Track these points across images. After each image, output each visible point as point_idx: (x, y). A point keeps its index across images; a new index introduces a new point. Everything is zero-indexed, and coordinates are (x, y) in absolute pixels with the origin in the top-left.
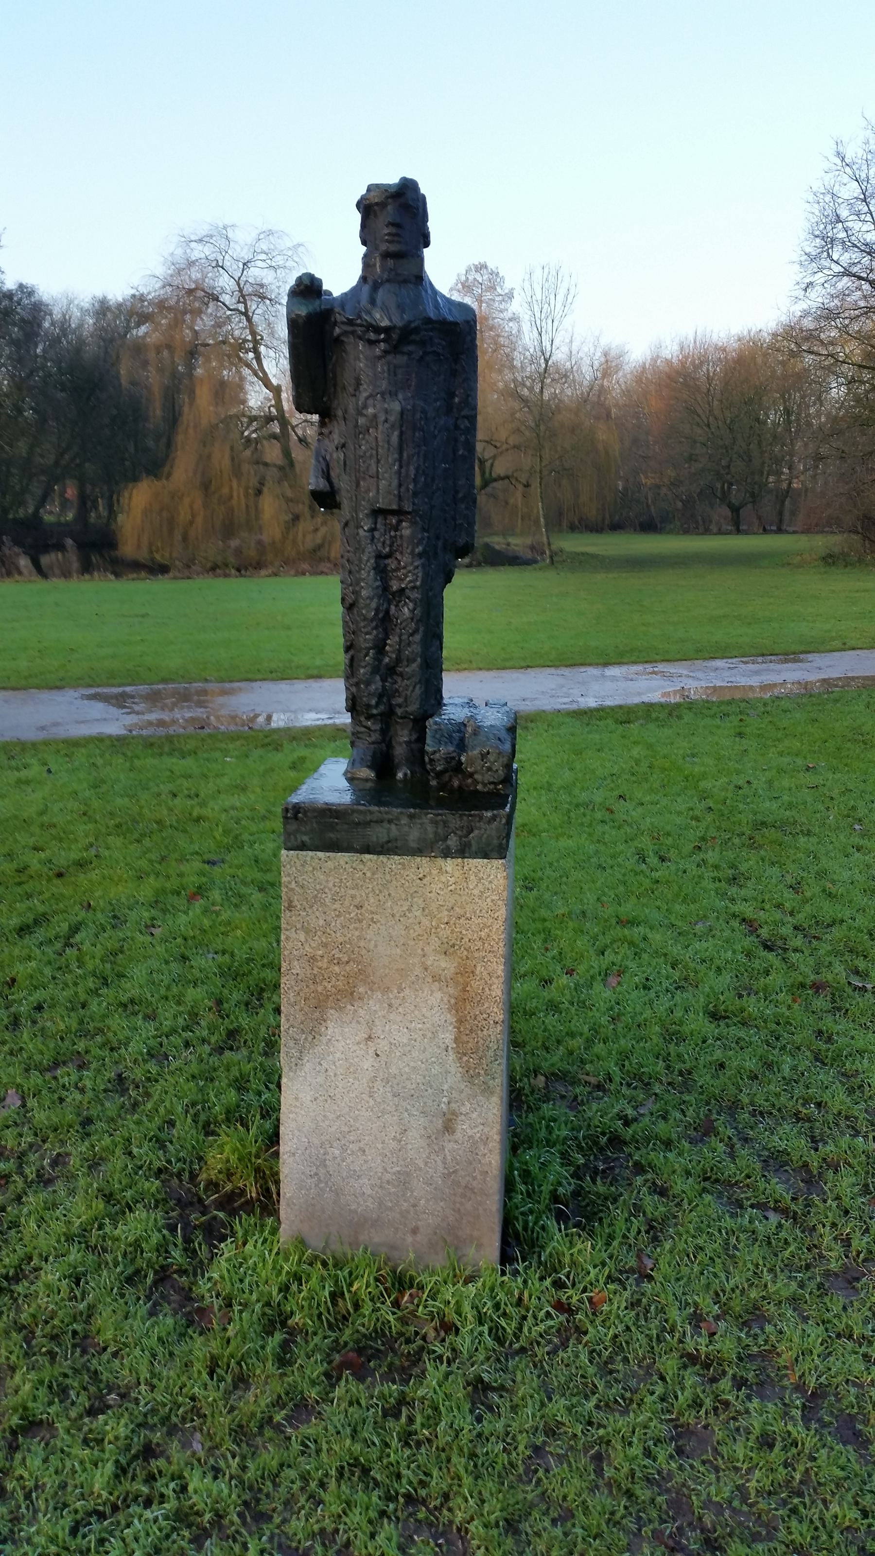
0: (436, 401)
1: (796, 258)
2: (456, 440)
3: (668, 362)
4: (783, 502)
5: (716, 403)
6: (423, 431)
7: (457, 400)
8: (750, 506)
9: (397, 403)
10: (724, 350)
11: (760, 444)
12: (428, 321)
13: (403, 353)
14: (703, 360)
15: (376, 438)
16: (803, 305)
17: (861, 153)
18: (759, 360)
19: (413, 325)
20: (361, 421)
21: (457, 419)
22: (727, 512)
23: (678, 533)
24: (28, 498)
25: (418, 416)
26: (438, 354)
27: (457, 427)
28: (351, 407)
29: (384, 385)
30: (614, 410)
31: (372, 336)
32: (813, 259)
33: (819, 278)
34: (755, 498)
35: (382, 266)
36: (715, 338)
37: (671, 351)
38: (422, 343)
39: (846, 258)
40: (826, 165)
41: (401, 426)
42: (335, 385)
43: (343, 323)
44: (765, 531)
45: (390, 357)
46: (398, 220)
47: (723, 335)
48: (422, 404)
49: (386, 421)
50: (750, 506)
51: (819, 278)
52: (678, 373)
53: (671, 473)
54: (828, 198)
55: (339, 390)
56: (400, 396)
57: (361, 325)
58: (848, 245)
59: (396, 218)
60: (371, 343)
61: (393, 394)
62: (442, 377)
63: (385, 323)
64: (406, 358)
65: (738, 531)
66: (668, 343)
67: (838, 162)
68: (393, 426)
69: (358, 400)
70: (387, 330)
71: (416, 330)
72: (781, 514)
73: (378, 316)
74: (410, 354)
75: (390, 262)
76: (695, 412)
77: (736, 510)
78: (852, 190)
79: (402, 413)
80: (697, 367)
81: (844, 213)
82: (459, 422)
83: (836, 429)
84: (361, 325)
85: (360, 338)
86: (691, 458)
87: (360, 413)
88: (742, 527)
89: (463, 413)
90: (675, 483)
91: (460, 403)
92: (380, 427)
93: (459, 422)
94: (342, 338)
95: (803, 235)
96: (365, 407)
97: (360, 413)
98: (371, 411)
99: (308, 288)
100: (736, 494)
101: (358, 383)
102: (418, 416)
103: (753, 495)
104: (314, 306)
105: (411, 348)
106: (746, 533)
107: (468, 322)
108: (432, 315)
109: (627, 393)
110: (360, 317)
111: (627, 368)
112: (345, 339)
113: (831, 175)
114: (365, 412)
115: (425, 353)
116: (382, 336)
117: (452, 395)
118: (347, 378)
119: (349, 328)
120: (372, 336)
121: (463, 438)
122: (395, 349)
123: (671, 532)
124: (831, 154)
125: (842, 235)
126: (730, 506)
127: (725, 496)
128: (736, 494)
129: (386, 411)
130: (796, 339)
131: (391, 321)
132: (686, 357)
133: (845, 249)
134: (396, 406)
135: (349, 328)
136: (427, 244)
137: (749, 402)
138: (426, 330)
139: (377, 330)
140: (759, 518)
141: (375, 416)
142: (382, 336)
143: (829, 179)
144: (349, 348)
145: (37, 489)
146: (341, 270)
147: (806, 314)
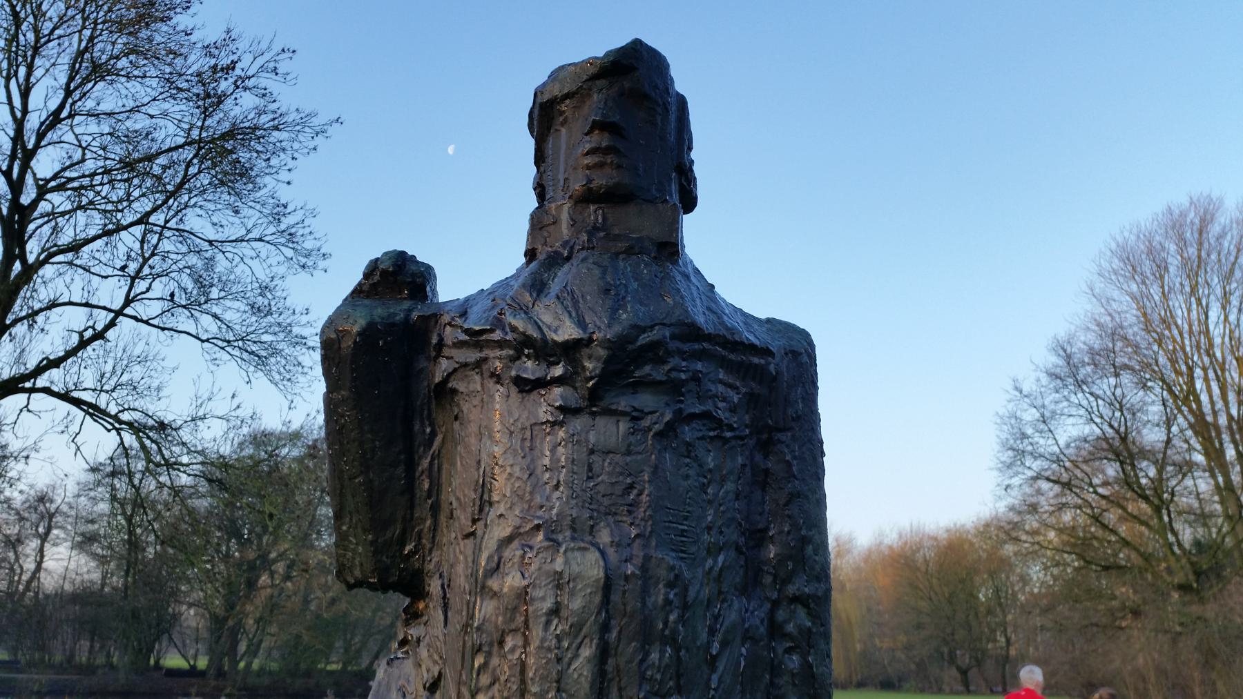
0: (713, 551)
1: (992, 465)
2: (775, 669)
3: (891, 548)
4: (1004, 668)
5: (934, 581)
6: (671, 640)
7: (772, 552)
8: (975, 670)
9: (593, 556)
10: (936, 539)
11: (976, 614)
12: (691, 332)
13: (609, 412)
14: (919, 547)
15: (523, 666)
16: (1010, 501)
17: (1034, 388)
18: (966, 547)
19: (644, 339)
20: (485, 610)
21: (776, 604)
22: (954, 672)
23: (915, 692)
24: (364, 654)
25: (659, 594)
26: (719, 424)
27: (775, 630)
28: (460, 568)
29: (558, 503)
30: (848, 586)
31: (530, 368)
32: (1009, 466)
33: (1016, 481)
34: (979, 663)
35: (573, 223)
36: (927, 530)
37: (891, 538)
38: (673, 388)
39: (1037, 465)
40: (1008, 397)
41: (605, 628)
42: (435, 509)
43: (460, 345)
44: (992, 692)
45: (578, 423)
46: (616, 118)
47: (933, 527)
48: (671, 559)
49: (555, 611)
50: (975, 670)
51: (1016, 481)
52: (900, 556)
53: (902, 638)
54: (1013, 421)
55: (443, 519)
56: (604, 537)
57: (501, 344)
58: (1036, 456)
59: (619, 138)
60: (526, 386)
61: (583, 532)
62: (730, 486)
63: (567, 332)
64: (623, 426)
65: (969, 692)
66: (888, 531)
67: (1017, 394)
68: (576, 628)
69: (478, 550)
70: (570, 350)
71: (654, 353)
72: (1004, 677)
73: (547, 318)
74: (635, 416)
75: (593, 214)
76: (917, 588)
77: (964, 672)
78: (1031, 415)
79: (607, 586)
80: (914, 552)
81: (1029, 431)
82: (781, 615)
83: (1048, 604)
84: (501, 344)
85: (497, 378)
86: (919, 626)
87: (481, 589)
88: (972, 688)
89: (791, 589)
90: (908, 648)
91: (781, 560)
92: (537, 632)
93: (781, 615)
94: (452, 384)
95: (997, 447)
96: (496, 569)
97: (481, 589)
98: (512, 581)
99: (398, 278)
100: (964, 659)
101: (484, 504)
102: (659, 594)
103: (977, 659)
104: (399, 309)
105: (646, 400)
106: (975, 693)
107: (795, 354)
108: (701, 320)
109: (857, 569)
110: (498, 323)
111: (855, 552)
112: (461, 387)
113: (1012, 404)
114: (494, 584)
115: (681, 418)
116: (558, 371)
117: (758, 537)
118: (458, 489)
119: (472, 356)
120: (530, 368)
121: (794, 662)
122: (596, 401)
123: (908, 691)
124: (1010, 387)
125: (1030, 448)
126: (959, 669)
127: (952, 659)
128: (964, 659)
129: (559, 582)
130: (1003, 531)
131: (581, 324)
132: (906, 543)
133: (1036, 458)
134: (590, 566)
135: (472, 356)
136: (689, 202)
137: (962, 581)
138: (682, 355)
139: (545, 351)
140: (986, 680)
141: (523, 595)
142: (558, 371)
143: (1011, 406)
144: (468, 408)
145: (373, 646)
146: (477, 249)
147: (1012, 508)
